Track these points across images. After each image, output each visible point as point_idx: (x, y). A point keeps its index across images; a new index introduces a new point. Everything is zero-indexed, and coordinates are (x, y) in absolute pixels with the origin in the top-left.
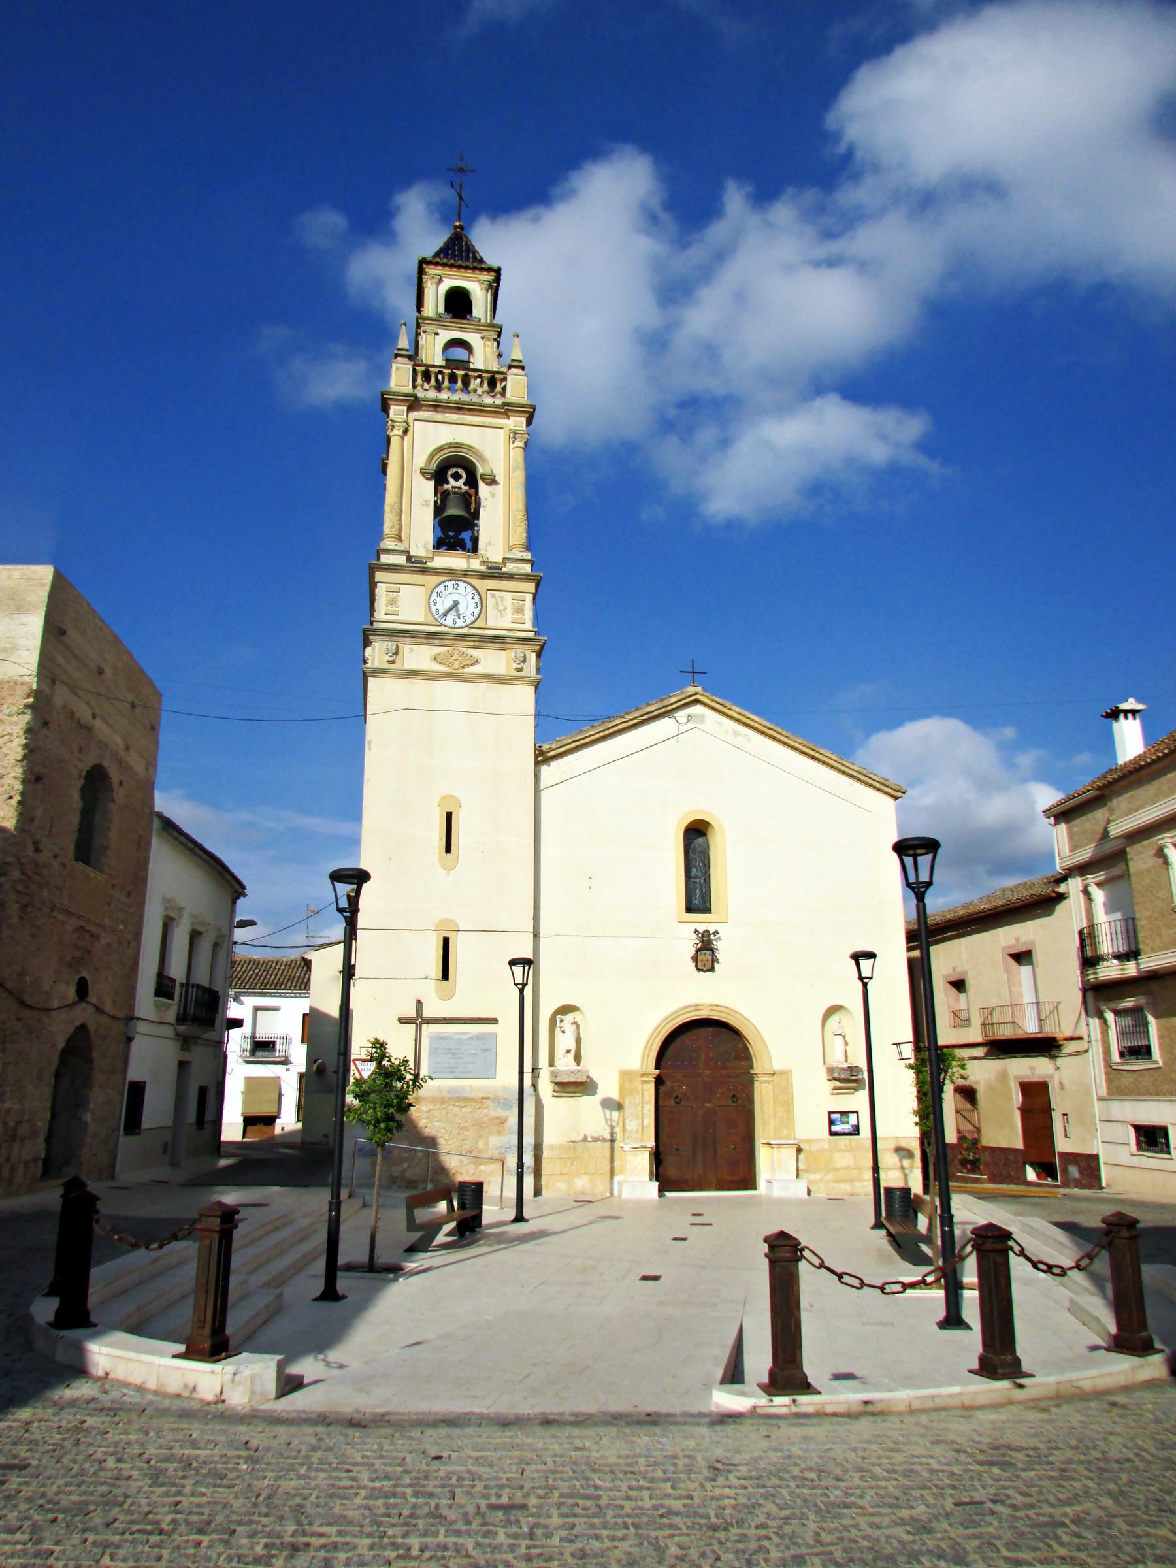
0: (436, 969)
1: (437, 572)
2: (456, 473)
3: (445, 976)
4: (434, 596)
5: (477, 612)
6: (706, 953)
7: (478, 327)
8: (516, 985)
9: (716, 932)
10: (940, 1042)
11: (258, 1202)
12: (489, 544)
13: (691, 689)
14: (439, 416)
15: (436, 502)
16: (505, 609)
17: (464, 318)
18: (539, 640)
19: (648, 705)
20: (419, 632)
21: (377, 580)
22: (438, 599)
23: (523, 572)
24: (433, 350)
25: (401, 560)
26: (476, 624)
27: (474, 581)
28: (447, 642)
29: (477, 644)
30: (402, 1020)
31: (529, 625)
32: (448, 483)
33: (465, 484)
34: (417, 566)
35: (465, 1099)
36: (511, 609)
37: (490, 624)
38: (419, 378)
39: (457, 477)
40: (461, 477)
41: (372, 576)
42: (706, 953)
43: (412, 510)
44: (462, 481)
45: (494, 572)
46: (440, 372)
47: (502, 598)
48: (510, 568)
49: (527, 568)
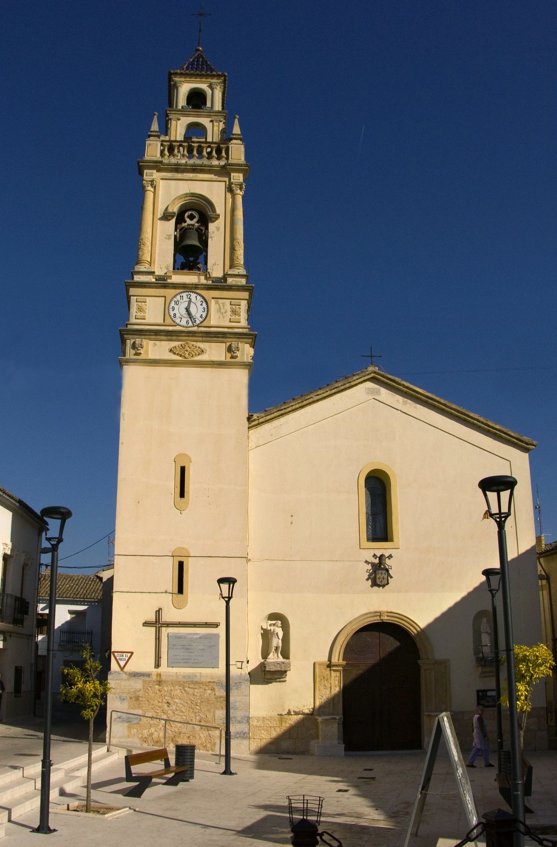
0: (171, 584)
1: (175, 286)
2: (193, 220)
3: (181, 590)
4: (173, 304)
5: (204, 315)
6: (379, 574)
7: (211, 113)
8: (223, 598)
9: (390, 557)
10: (60, 521)
11: (22, 757)
12: (215, 264)
13: (371, 369)
14: (179, 176)
15: (175, 236)
16: (226, 312)
17: (200, 108)
18: (251, 335)
19: (337, 382)
20: (161, 331)
21: (131, 293)
22: (176, 307)
23: (240, 284)
24: (178, 129)
25: (151, 279)
26: (204, 324)
27: (203, 293)
28: (182, 338)
29: (204, 339)
30: (146, 624)
31: (244, 322)
32: (185, 222)
33: (198, 222)
34: (162, 283)
35: (196, 683)
36: (229, 312)
37: (213, 323)
38: (166, 152)
39: (191, 217)
40: (195, 217)
41: (128, 292)
42: (379, 574)
43: (158, 244)
44: (196, 220)
45: (220, 284)
46: (181, 145)
47: (224, 304)
48: (230, 281)
49: (243, 281)
